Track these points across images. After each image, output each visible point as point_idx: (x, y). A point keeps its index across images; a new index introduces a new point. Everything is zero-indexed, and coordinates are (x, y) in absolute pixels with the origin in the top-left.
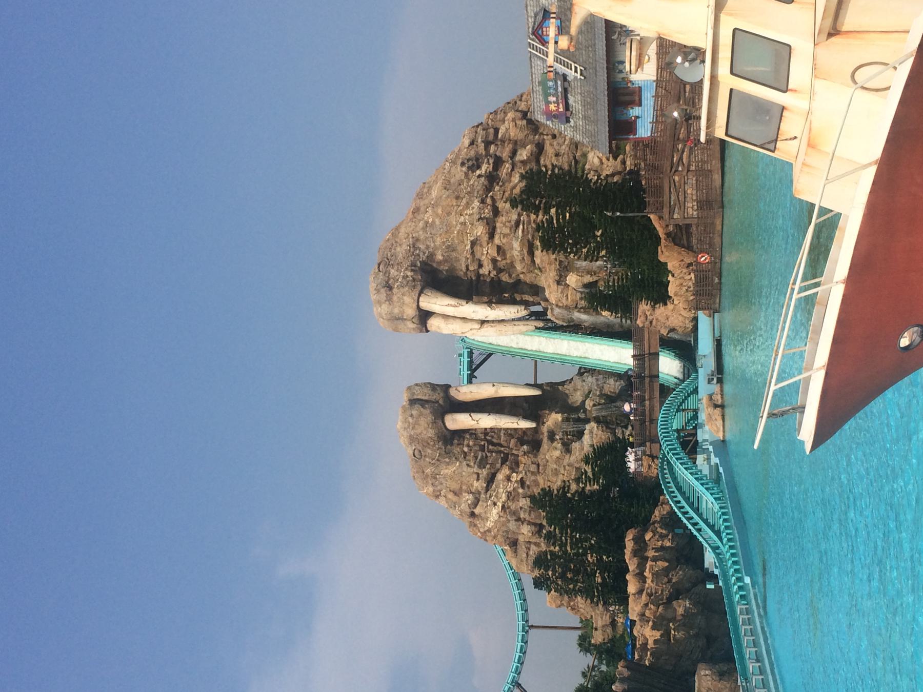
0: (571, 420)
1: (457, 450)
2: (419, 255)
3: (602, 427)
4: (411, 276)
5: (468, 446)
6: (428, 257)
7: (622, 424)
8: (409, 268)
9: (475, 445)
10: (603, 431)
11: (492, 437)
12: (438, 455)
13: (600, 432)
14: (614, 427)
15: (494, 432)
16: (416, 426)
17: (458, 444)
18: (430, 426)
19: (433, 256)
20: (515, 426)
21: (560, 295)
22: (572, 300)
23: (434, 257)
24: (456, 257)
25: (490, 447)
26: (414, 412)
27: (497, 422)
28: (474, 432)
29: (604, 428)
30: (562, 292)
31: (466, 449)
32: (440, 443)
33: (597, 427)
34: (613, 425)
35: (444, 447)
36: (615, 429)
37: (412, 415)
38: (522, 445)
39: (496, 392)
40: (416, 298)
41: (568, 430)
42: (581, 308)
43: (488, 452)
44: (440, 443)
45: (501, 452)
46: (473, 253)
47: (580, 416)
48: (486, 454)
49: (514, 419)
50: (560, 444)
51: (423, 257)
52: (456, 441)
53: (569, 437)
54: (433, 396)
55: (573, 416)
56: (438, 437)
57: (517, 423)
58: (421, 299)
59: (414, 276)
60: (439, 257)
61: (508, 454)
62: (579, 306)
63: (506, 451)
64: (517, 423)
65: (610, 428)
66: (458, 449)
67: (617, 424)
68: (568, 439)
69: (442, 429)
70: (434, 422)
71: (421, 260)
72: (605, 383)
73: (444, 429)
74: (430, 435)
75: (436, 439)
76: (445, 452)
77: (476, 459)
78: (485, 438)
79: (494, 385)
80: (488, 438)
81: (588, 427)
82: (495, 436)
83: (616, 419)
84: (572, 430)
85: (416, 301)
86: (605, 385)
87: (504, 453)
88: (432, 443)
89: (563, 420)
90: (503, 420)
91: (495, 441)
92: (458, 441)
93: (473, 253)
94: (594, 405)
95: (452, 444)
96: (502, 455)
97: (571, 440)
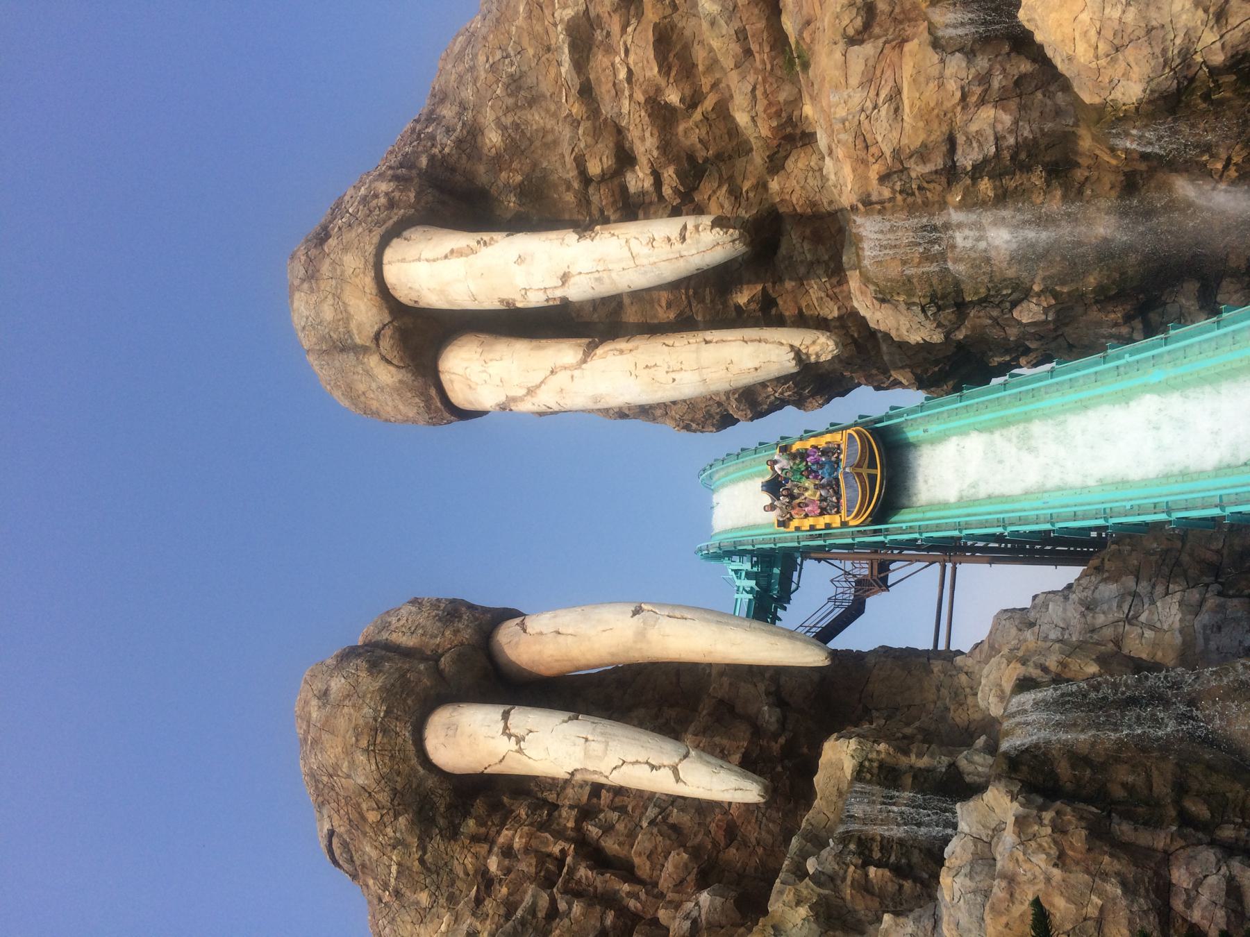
0: (908, 780)
1: (463, 861)
2: (432, 138)
3: (1059, 829)
4: (387, 194)
5: (507, 852)
6: (459, 142)
7: (1228, 832)
8: (390, 172)
9: (527, 850)
10: (1060, 860)
11: (608, 829)
12: (394, 869)
13: (1040, 860)
14: (1160, 841)
15: (622, 810)
16: (325, 736)
17: (475, 839)
18: (364, 743)
19: (474, 137)
20: (662, 783)
21: (857, 97)
22: (925, 115)
23: (479, 139)
24: (545, 132)
25: (583, 872)
26: (337, 684)
27: (587, 754)
28: (552, 797)
29: (1078, 838)
30: (869, 80)
31: (493, 864)
32: (402, 820)
33: (1020, 822)
34: (1153, 822)
35: (414, 841)
36: (1167, 858)
37: (324, 695)
38: (702, 885)
39: (641, 635)
40: (370, 249)
41: (879, 830)
42: (978, 171)
43: (566, 891)
44: (402, 820)
45: (608, 900)
46: (586, 92)
47: (963, 763)
48: (553, 901)
49: (661, 751)
50: (803, 911)
51: (446, 143)
52: (471, 822)
53: (872, 871)
54: (434, 636)
55: (924, 762)
56: (395, 792)
57: (675, 770)
58: (389, 254)
59: (397, 194)
60: (493, 138)
61: (636, 918)
62: (967, 158)
63: (632, 904)
64: (675, 770)
65: (1120, 847)
66: (469, 861)
67: (1185, 819)
68: (865, 887)
69: (405, 760)
70: (379, 729)
71: (436, 151)
72: (1130, 620)
73: (414, 761)
74: (361, 781)
75: (384, 797)
76: (422, 861)
77: (508, 917)
78: (578, 828)
79: (636, 612)
80: (593, 830)
81: (968, 816)
82: (620, 827)
83: (1181, 789)
84: (898, 832)
85: (371, 260)
86: (1133, 632)
87: (622, 911)
88: (372, 817)
89: (859, 774)
90: (613, 744)
91: (610, 845)
92: (481, 823)
93: (586, 92)
94: (1025, 684)
95: (453, 833)
96: (610, 918)
97: (881, 896)
